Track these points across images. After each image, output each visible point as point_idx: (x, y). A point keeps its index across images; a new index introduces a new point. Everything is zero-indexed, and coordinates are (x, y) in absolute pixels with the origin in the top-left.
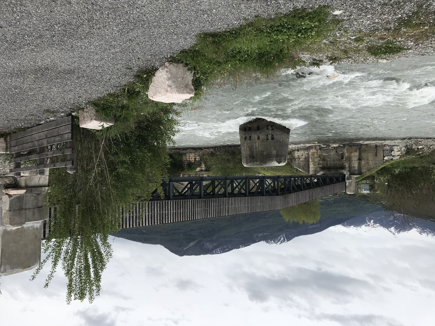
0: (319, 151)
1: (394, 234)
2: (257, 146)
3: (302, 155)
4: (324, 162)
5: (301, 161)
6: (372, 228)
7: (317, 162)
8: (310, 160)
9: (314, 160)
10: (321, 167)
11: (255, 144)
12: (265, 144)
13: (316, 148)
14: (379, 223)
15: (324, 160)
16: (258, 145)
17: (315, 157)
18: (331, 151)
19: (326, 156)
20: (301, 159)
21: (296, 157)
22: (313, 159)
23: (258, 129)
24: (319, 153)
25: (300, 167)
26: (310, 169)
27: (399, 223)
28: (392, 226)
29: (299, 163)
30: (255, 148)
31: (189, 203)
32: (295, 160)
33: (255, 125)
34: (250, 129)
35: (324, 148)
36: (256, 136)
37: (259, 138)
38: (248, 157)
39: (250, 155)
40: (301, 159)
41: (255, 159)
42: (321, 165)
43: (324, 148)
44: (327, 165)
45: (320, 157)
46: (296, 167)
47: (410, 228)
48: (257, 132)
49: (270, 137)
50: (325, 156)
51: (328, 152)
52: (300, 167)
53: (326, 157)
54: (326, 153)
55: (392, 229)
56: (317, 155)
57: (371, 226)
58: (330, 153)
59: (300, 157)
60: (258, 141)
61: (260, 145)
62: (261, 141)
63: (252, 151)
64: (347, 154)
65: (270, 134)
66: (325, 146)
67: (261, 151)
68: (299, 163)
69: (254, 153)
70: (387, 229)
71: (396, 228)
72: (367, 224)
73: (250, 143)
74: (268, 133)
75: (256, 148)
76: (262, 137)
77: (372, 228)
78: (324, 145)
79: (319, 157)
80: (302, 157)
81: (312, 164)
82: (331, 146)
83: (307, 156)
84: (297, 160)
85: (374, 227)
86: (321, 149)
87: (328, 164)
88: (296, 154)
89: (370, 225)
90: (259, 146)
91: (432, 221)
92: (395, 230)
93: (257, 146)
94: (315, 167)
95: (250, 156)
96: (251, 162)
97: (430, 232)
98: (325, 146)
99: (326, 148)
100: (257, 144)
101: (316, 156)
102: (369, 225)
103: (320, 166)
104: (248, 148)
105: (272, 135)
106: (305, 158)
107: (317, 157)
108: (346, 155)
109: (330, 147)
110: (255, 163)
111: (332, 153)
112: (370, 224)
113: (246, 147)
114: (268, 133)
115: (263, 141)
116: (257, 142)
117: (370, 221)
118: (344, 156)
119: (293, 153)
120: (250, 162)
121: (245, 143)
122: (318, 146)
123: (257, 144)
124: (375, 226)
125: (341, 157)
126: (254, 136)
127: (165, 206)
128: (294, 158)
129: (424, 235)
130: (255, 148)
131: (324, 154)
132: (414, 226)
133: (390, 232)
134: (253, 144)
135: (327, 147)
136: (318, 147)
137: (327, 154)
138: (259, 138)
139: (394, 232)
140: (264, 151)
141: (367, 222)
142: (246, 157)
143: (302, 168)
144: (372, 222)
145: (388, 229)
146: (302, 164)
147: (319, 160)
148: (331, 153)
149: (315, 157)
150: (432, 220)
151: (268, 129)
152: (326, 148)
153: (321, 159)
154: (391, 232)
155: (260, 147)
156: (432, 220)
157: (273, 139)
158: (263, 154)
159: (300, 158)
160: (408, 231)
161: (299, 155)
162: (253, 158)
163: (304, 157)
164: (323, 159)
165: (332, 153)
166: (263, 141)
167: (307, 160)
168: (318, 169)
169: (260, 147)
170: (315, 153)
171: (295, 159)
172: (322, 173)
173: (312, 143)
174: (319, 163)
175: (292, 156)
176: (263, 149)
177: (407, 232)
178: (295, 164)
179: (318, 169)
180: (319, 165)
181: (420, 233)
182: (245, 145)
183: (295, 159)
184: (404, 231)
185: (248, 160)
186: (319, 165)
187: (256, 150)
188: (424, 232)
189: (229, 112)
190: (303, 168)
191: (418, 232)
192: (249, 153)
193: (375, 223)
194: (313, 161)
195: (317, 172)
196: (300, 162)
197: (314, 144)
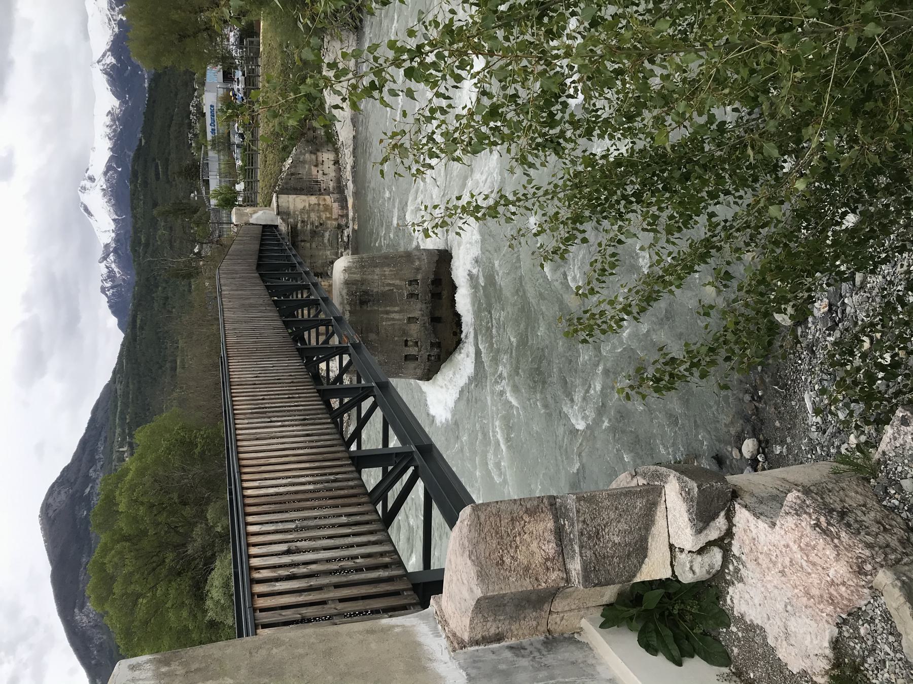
0: (335, 223)
1: (99, 62)
2: (393, 316)
3: (324, 174)
5: (310, 169)
6: (107, 15)
7: (309, 217)
8: (313, 199)
9: (313, 210)
10: (297, 226)
11: (396, 309)
12: (396, 339)
13: (342, 216)
14: (120, 32)
15: (314, 233)
16: (393, 319)
20: (314, 170)
21: (319, 154)
22: (317, 207)
23: (435, 320)
24: (329, 222)
25: (295, 167)
26: (292, 197)
27: (126, 75)
28: (118, 59)
29: (304, 162)
30: (388, 308)
31: (277, 444)
32: (311, 153)
33: (443, 313)
34: (436, 296)
36: (417, 314)
37: (411, 320)
39: (369, 295)
40: (314, 170)
41: (358, 308)
42: (302, 227)
44: (302, 241)
46: (294, 151)
47: (118, 93)
49: (413, 351)
50: (323, 236)
51: (331, 245)
52: (295, 167)
53: (320, 239)
54: (329, 240)
55: (110, 60)
56: (326, 218)
57: (112, 15)
59: (320, 166)
62: (404, 327)
63: (378, 301)
65: (419, 351)
66: (345, 239)
67: (377, 326)
68: (304, 162)
69: (374, 304)
70: (108, 47)
71: (113, 67)
72: (114, 6)
74: (421, 346)
75: (387, 313)
76: (415, 330)
77: (107, 15)
79: (322, 222)
80: (321, 172)
83: (323, 186)
84: (314, 157)
85: (110, 20)
86: (340, 228)
87: (303, 244)
88: (327, 157)
89: (113, 13)
91: (141, 140)
92: (108, 65)
93: (393, 316)
95: (366, 293)
96: (350, 296)
97: (115, 131)
98: (345, 239)
99: (340, 240)
100: (396, 316)
102: (113, 9)
103: (299, 225)
104: (387, 288)
106: (317, 181)
107: (319, 217)
108: (323, 283)
110: (348, 308)
111: (328, 253)
112: (116, 13)
113: (389, 285)
114: (421, 346)
115: (404, 333)
116: (401, 317)
117: (123, 12)
119: (330, 147)
120: (350, 293)
121: (401, 279)
122: (347, 223)
123: (396, 316)
124: (113, 22)
125: (319, 271)
126: (418, 309)
128: (318, 150)
129: (108, 120)
130: (388, 308)
131: (327, 235)
132: (124, 103)
133: (102, 54)
136: (343, 222)
137: (326, 241)
138: (411, 320)
139: (103, 62)
140: (378, 333)
141: (121, 7)
142: (363, 282)
143: (292, 170)
144: (120, 16)
145: (109, 50)
146: (303, 171)
147: (312, 223)
150: (143, 141)
152: (340, 240)
153: (317, 227)
154: (104, 55)
155: (389, 323)
156: (143, 141)
157: (407, 358)
158: (372, 332)
159: (316, 166)
160: (111, 90)
161: (326, 166)
162: (363, 303)
163: (320, 177)
165: (328, 253)
166: (405, 333)
167: (310, 188)
168: (292, 220)
169: (389, 323)
170: (331, 213)
171: (314, 152)
172: (283, 229)
173: (354, 215)
175: (322, 145)
177: (109, 88)
178: (303, 151)
180: (303, 222)
181: (109, 112)
182: (397, 282)
183: (315, 154)
184: (109, 84)
185: (355, 287)
186: (303, 222)
187: (383, 312)
188: (113, 120)
190: (292, 174)
191: (110, 109)
192: (375, 290)
193: (120, 24)
194: (312, 208)
196: (307, 166)
197: (354, 220)
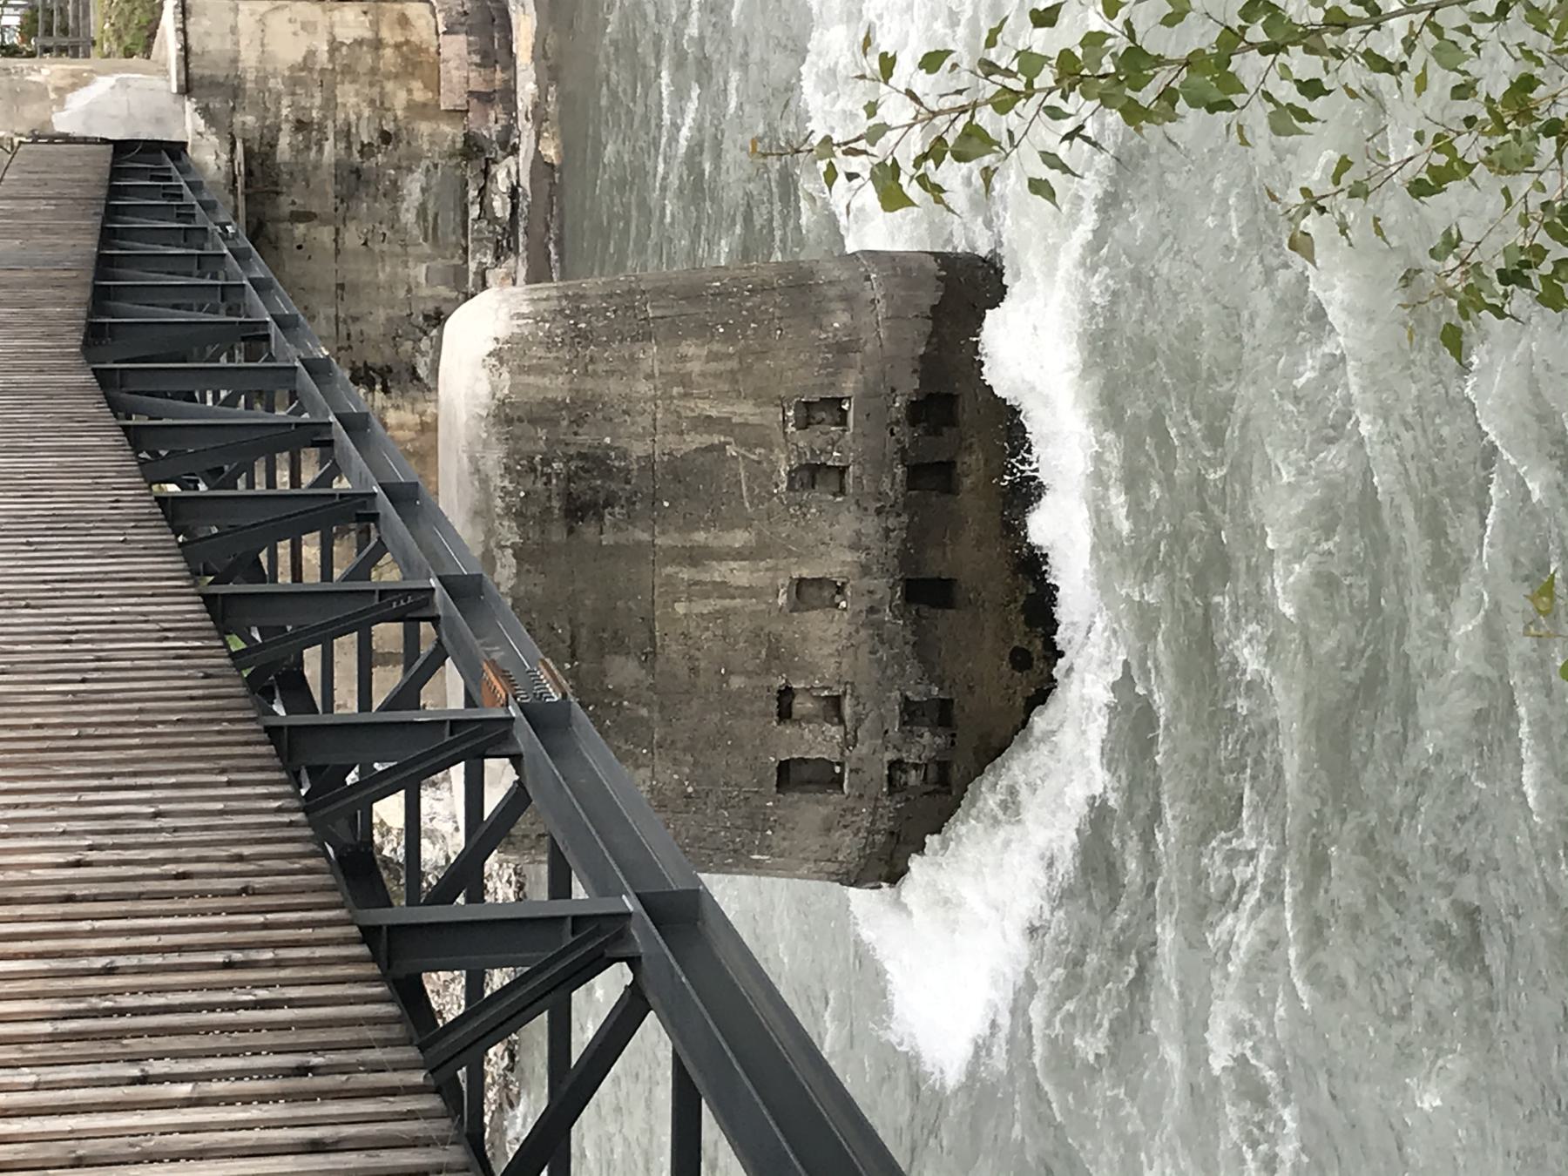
0: (451, 132)
2: (718, 572)
4: (330, 189)
7: (330, 104)
9: (348, 71)
10: (273, 146)
11: (740, 538)
12: (737, 682)
13: (485, 98)
15: (353, 180)
17: (390, 86)
18: (439, 263)
19: (395, 210)
24: (424, 127)
30: (700, 537)
35: (482, 191)
36: (837, 563)
38: (586, 438)
39: (608, 473)
41: (558, 535)
43: (482, 191)
45: (386, 137)
48: (880, 585)
50: (394, 192)
51: (432, 233)
53: (383, 207)
54: (422, 212)
58: (427, 248)
60: (783, 581)
61: (723, 614)
62: (779, 627)
63: (655, 500)
64: (401, 427)
65: (850, 742)
66: (500, 206)
67: (648, 621)
69: (630, 518)
73: (762, 474)
74: (859, 721)
75: (695, 556)
78: (514, 192)
79: (389, 127)
81: (311, 54)
82: (501, 271)
90: (714, 604)
94: (276, 84)
95: (594, 462)
98: (500, 206)
99: (474, 212)
100: (739, 574)
101: (399, 99)
103: (284, 141)
104: (695, 441)
105: (824, 777)
107: (380, 106)
109: (488, 260)
110: (509, 533)
113: (708, 423)
114: (859, 721)
115: (774, 655)
118: (385, 390)
120: (523, 466)
121: (759, 397)
122: (509, 130)
123: (739, 574)
125: (375, 360)
127: (230, 721)
130: (700, 537)
131: (413, 186)
134: (747, 524)
135: (494, 220)
137: (408, 217)
140: (649, 656)
148: (421, 259)
149: (390, 86)
151: (911, 712)
152: (474, 212)
153: (366, 150)
157: (788, 775)
162: (578, 510)
164: (357, 172)
166: (776, 653)
168: (250, 119)
172: (210, 159)
174: (321, 128)
176: (674, 649)
179: (250, 119)
180: (301, 125)
182: (745, 411)
185: (542, 433)
186: (301, 125)
189: (1268, 530)
192: (639, 449)
195: (215, 104)
